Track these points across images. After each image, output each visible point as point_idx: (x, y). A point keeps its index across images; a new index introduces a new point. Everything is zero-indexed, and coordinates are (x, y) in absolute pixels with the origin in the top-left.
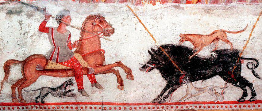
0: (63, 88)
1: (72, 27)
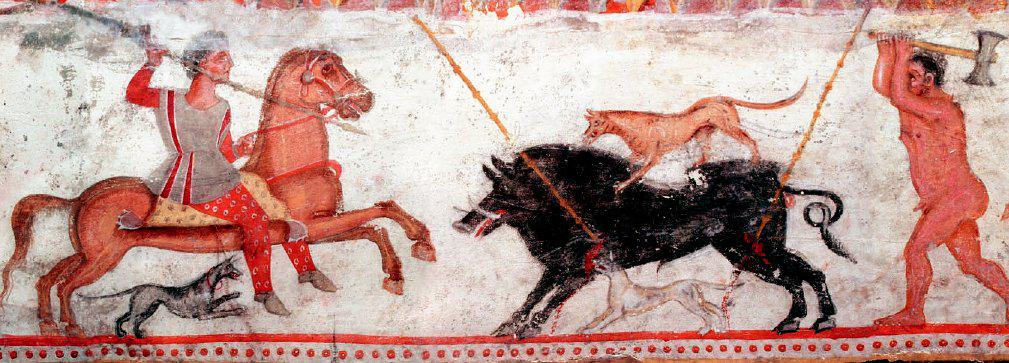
1: (236, 87)
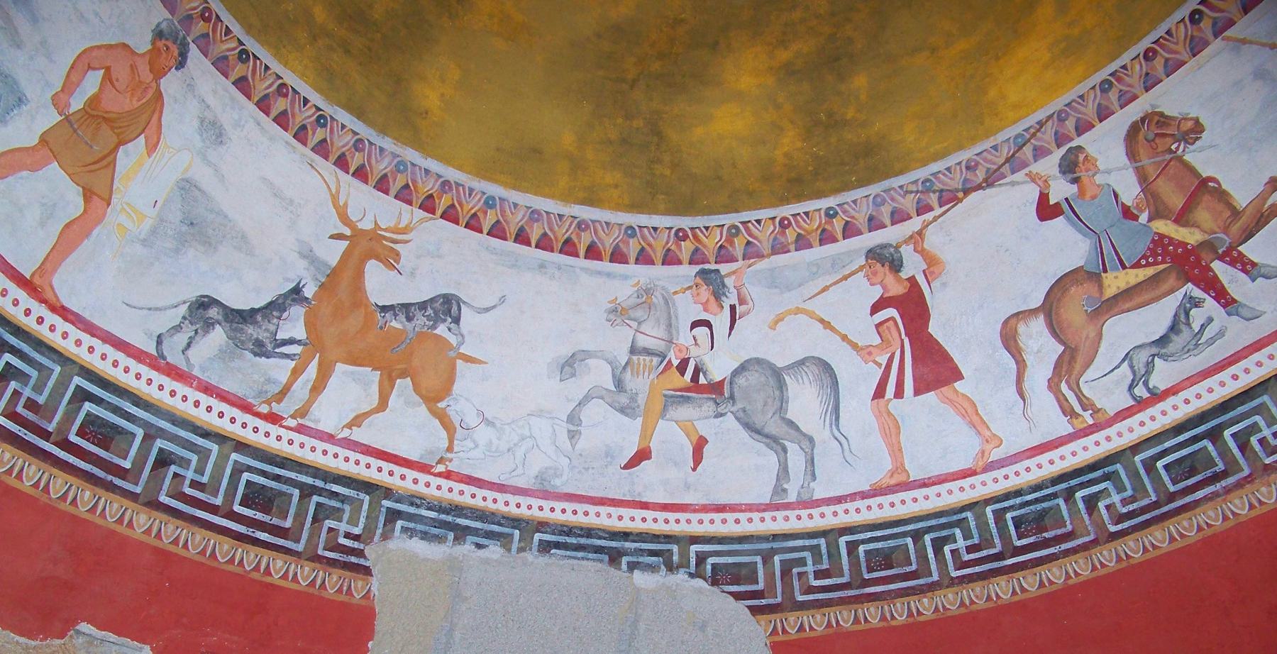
0: (1183, 327)
1: (1108, 172)
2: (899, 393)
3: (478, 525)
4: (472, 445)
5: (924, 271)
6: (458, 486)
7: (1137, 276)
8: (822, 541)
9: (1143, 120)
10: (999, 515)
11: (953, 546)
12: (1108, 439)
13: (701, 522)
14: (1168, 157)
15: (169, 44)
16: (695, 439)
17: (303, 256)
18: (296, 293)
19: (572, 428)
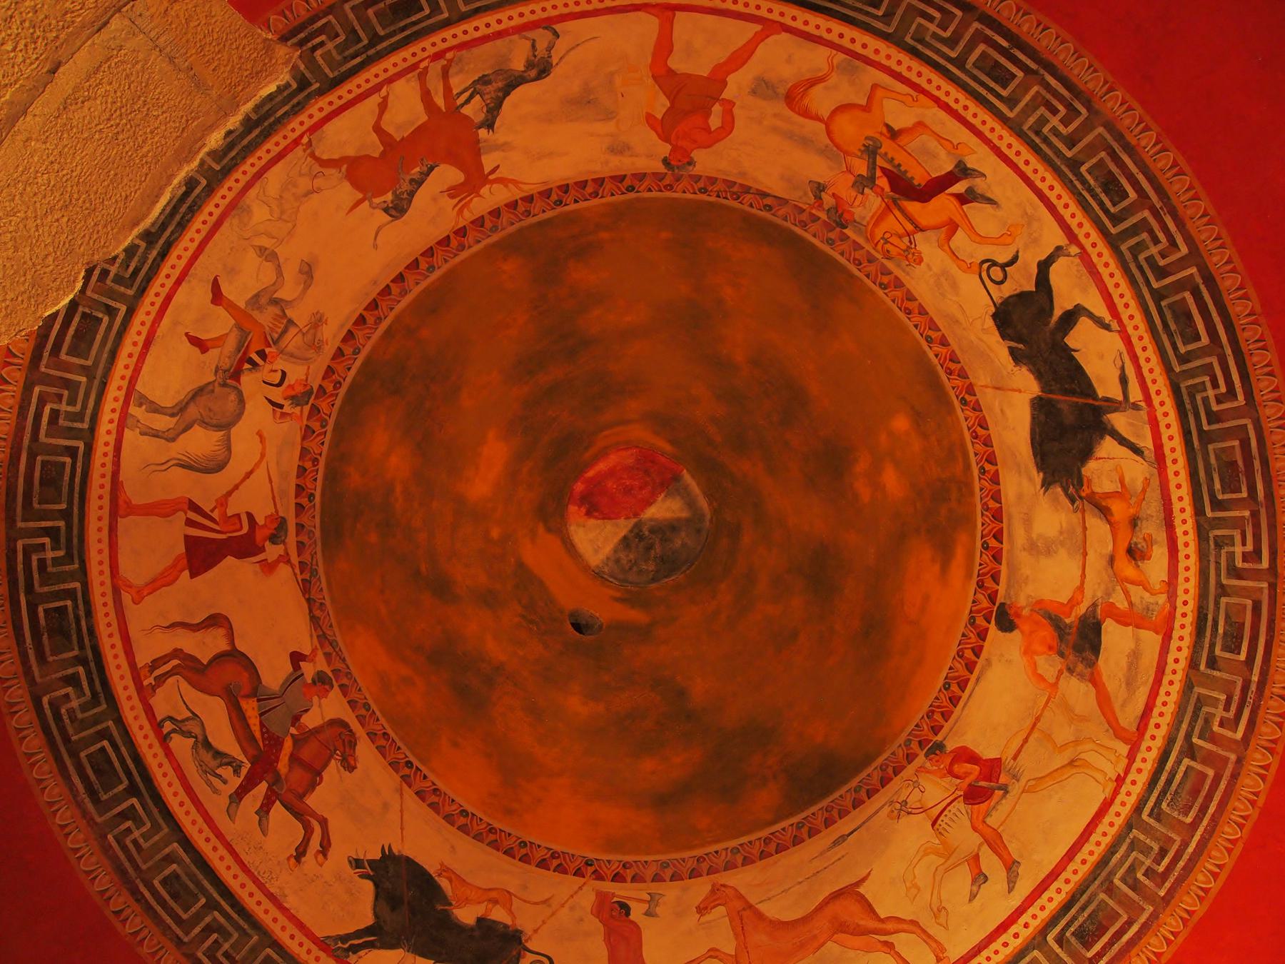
0: (219, 761)
1: (320, 706)
2: (189, 523)
3: (245, 142)
4: (303, 172)
5: (266, 560)
6: (284, 143)
7: (255, 725)
8: (86, 426)
9: (351, 731)
10: (71, 594)
11: (48, 546)
12: (129, 698)
13: (143, 324)
14: (332, 748)
15: (680, 163)
16: (209, 344)
17: (505, 144)
18: (490, 125)
19: (267, 252)
